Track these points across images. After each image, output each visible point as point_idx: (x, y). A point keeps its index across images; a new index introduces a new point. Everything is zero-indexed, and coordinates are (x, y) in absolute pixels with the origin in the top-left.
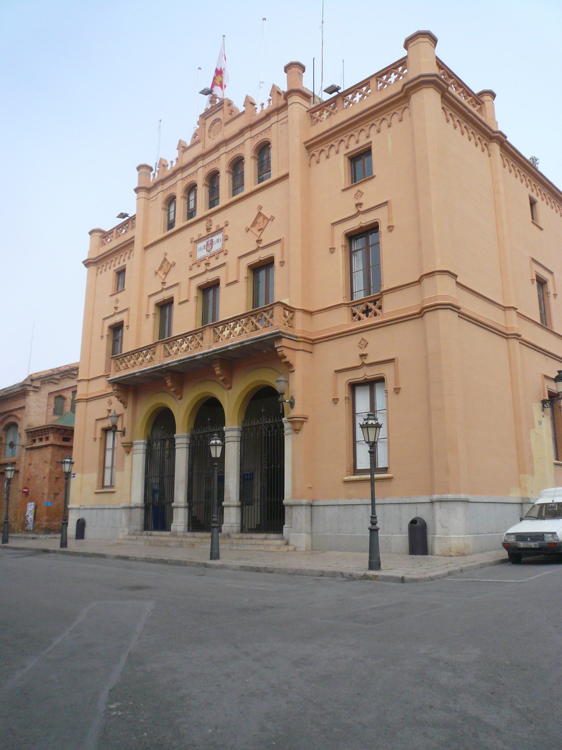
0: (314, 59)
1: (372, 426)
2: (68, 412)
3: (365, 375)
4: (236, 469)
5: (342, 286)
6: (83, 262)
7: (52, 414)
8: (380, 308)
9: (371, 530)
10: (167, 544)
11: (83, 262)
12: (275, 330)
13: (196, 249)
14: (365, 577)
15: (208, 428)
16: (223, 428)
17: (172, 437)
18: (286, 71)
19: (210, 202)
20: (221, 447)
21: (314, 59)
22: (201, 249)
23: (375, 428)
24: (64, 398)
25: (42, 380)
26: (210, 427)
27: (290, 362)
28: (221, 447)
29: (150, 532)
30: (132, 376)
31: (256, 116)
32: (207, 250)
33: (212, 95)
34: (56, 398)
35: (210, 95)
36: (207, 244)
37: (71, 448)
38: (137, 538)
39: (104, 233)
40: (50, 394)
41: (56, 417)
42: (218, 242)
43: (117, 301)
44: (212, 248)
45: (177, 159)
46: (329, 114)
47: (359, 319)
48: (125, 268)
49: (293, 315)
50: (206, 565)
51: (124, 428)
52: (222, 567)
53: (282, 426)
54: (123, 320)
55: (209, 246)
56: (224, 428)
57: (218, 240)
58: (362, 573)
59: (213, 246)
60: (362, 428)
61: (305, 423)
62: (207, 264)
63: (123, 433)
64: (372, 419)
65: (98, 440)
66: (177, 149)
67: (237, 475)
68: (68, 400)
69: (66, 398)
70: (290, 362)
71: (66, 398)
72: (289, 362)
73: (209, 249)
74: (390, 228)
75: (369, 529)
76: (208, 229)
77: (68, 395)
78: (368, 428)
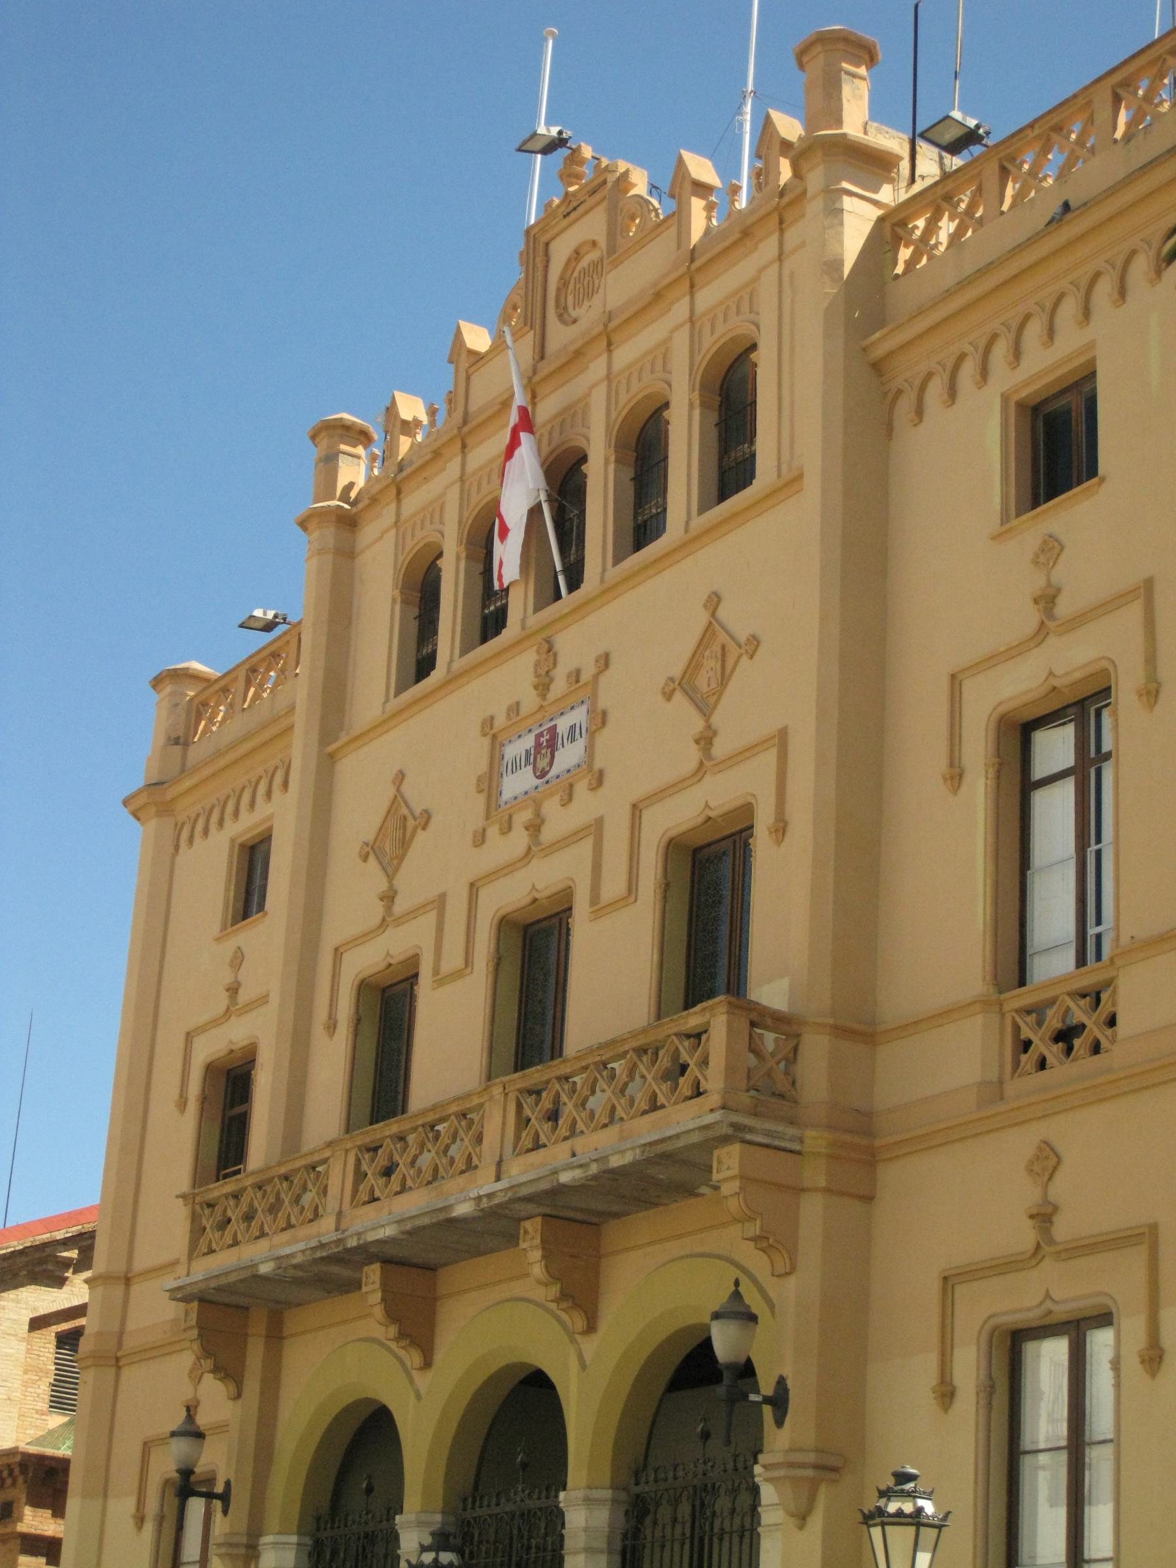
0: (916, 7)
3: (1048, 1295)
5: (980, 927)
6: (126, 803)
7: (44, 1405)
8: (1112, 1022)
11: (126, 803)
13: (500, 765)
15: (515, 1494)
16: (557, 1496)
17: (550, 1502)
18: (801, 66)
19: (723, 473)
21: (916, 7)
22: (515, 767)
23: (912, 1529)
25: (297, 1155)
26: (523, 1491)
31: (714, 233)
32: (534, 767)
33: (569, 151)
35: (563, 152)
36: (538, 745)
39: (204, 685)
40: (38, 1324)
41: (57, 1420)
42: (573, 740)
43: (238, 959)
44: (551, 764)
45: (451, 400)
46: (1068, 159)
47: (1042, 1064)
48: (270, 829)
53: (755, 1490)
54: (1105, 664)
55: (543, 751)
56: (562, 1495)
57: (573, 728)
59: (556, 753)
62: (535, 828)
65: (149, 1527)
66: (451, 361)
72: (564, 1296)
73: (542, 763)
74: (1151, 693)
76: (543, 686)
78: (922, 1529)
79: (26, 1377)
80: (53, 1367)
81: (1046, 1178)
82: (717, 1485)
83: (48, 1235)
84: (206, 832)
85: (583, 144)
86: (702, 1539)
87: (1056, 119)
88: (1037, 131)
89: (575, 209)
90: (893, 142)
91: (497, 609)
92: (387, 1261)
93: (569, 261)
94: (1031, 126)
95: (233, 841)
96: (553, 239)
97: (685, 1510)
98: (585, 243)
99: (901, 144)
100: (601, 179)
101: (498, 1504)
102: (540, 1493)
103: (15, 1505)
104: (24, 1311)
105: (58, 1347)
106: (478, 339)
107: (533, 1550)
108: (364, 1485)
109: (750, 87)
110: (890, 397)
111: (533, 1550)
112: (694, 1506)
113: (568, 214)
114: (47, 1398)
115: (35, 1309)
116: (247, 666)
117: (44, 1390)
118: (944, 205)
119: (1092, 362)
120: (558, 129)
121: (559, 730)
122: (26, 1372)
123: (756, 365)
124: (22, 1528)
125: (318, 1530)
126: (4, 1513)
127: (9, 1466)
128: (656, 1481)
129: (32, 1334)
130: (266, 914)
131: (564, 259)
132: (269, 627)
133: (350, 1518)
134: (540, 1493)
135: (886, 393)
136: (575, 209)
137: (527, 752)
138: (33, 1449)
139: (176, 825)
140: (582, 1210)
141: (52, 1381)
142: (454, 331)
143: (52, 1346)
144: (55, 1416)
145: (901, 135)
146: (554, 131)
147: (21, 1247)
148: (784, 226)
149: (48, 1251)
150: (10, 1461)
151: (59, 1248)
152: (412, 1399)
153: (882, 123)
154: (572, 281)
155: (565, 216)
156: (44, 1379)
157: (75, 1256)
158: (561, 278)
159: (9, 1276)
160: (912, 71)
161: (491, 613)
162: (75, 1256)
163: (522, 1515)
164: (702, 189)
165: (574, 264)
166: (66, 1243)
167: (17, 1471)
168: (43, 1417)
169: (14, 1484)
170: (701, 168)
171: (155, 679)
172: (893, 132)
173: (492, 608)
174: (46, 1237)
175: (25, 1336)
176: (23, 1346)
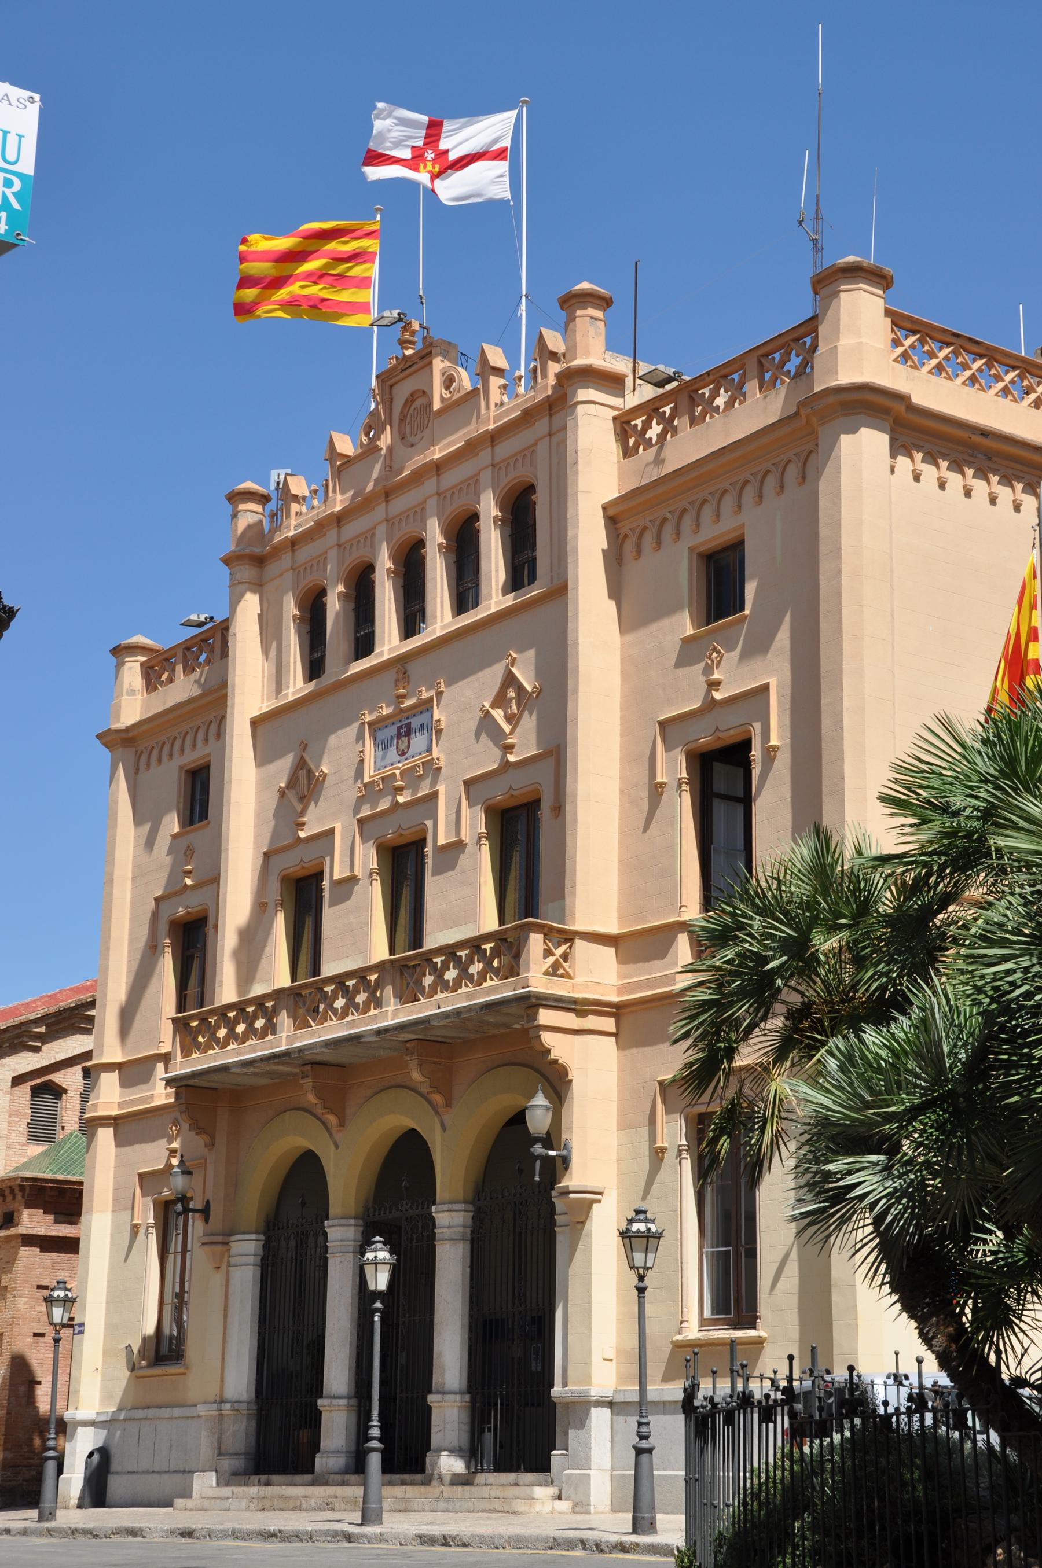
1: (639, 1235)
2: (71, 1134)
4: (460, 1311)
7: (23, 1139)
9: (639, 1452)
10: (298, 1503)
12: (523, 988)
14: (622, 1548)
20: (389, 1266)
24: (57, 1092)
27: (560, 1062)
28: (389, 1266)
29: (266, 1476)
30: (314, 902)
32: (397, 748)
34: (36, 1092)
37: (70, 1246)
38: (233, 1493)
41: (36, 1149)
44: (408, 747)
49: (570, 947)
50: (349, 1537)
51: (208, 1203)
52: (381, 1538)
54: (205, 907)
56: (433, 1208)
58: (614, 1538)
60: (623, 1238)
61: (595, 1206)
63: (205, 1212)
64: (639, 1221)
67: (462, 1326)
68: (70, 1094)
69: (65, 1091)
70: (560, 1062)
71: (65, 1091)
73: (403, 746)
75: (634, 1447)
77: (71, 1079)
79: (11, 1119)
80: (30, 1111)
81: (397, 1507)
82: (529, 1200)
83: (24, 1017)
84: (160, 760)
85: (413, 320)
86: (520, 1233)
87: (723, 372)
88: (712, 377)
89: (410, 366)
90: (620, 365)
91: (366, 635)
92: (611, 1404)
93: (407, 401)
94: (708, 373)
95: (181, 768)
96: (395, 383)
97: (292, 1243)
98: (418, 390)
99: (626, 364)
100: (429, 350)
101: (390, 1213)
102: (417, 1206)
103: (15, 1214)
104: (7, 1072)
105: (32, 1096)
106: (345, 446)
107: (415, 1241)
108: (300, 1201)
109: (524, 293)
110: (621, 537)
111: (415, 1241)
112: (515, 1214)
113: (406, 369)
114: (26, 1133)
115: (14, 1070)
116: (184, 646)
117: (23, 1128)
118: (653, 414)
119: (743, 535)
120: (398, 311)
121: (412, 726)
122: (10, 1116)
123: (535, 503)
124: (21, 1230)
125: (269, 1230)
126: (10, 1220)
127: (10, 1187)
128: (491, 1198)
129: (14, 1089)
130: (209, 823)
131: (403, 402)
132: (201, 624)
133: (291, 1222)
134: (417, 1206)
135: (618, 535)
136: (410, 366)
137: (392, 738)
138: (28, 1174)
139: (137, 752)
140: (443, 1037)
141: (29, 1121)
142: (328, 439)
143: (28, 1096)
144: (31, 1146)
145: (626, 358)
146: (395, 314)
147: (4, 1027)
148: (552, 412)
149: (24, 1029)
150: (12, 1184)
151: (32, 1025)
152: (333, 1147)
153: (614, 351)
154: (409, 415)
155: (403, 371)
156: (23, 1120)
157: (44, 1031)
158: (402, 412)
159: (719, 1406)
160: (633, 346)
161: (362, 636)
162: (44, 1031)
163: (407, 1218)
164: (499, 372)
165: (410, 404)
166: (36, 1022)
167: (17, 1191)
168: (24, 1147)
169: (14, 1198)
170: (496, 357)
171: (114, 649)
172: (621, 357)
173: (362, 633)
174: (22, 1018)
175: (9, 1090)
176: (8, 1097)
